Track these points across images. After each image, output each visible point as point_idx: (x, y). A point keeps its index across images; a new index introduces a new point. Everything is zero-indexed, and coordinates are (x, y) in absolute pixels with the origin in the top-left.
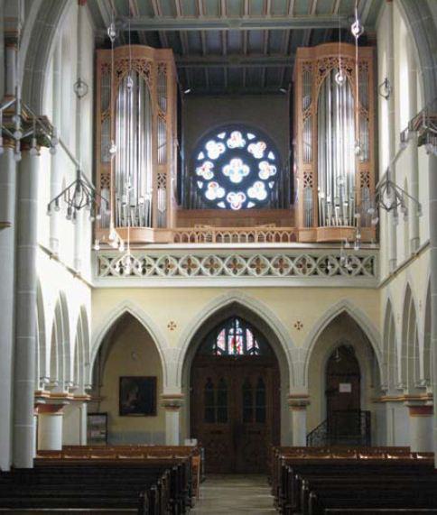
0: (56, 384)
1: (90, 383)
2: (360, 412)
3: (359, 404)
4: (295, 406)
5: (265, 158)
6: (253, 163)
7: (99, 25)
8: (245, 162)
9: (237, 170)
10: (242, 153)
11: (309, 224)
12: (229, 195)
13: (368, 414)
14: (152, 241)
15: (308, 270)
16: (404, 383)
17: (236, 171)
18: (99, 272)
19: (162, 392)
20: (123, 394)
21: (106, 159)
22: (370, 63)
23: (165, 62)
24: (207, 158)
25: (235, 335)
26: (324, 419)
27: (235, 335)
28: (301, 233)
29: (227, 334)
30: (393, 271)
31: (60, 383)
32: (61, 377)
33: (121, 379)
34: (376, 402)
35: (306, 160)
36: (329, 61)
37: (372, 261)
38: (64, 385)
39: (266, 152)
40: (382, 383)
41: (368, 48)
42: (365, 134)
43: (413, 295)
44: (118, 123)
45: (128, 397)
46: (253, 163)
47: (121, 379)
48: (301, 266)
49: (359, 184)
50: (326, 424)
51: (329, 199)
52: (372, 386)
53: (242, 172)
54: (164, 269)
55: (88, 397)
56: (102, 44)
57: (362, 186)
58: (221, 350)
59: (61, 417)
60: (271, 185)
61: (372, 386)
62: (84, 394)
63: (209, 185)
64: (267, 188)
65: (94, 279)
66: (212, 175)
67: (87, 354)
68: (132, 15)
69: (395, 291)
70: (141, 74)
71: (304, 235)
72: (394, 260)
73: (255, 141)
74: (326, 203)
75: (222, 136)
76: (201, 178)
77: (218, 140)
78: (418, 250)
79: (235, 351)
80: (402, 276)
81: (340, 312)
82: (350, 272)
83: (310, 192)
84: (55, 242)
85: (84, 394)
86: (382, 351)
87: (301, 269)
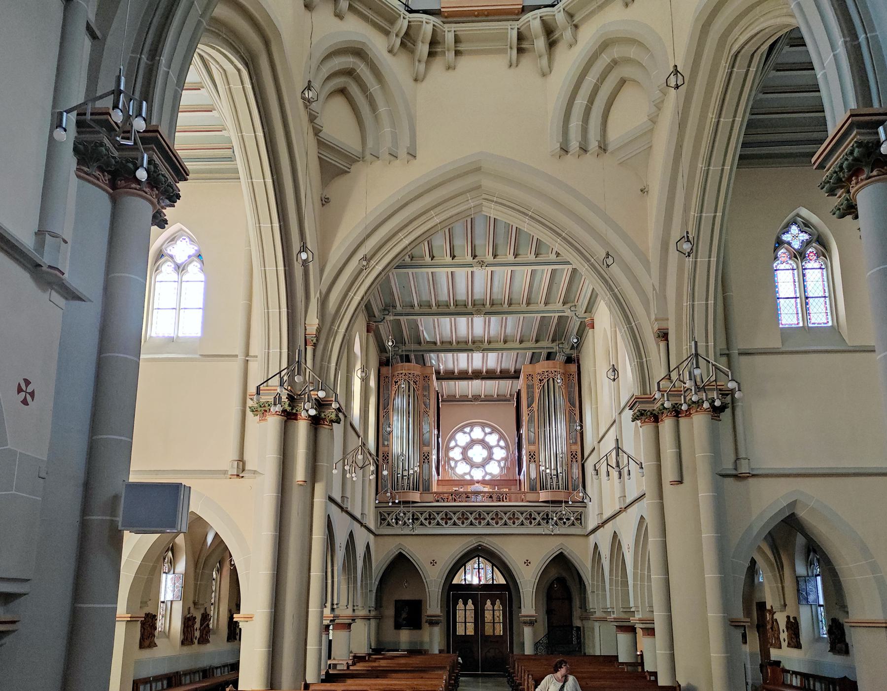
2: (571, 626)
4: (525, 623)
7: (382, 348)
8: (484, 459)
9: (478, 454)
13: (578, 628)
15: (533, 521)
16: (637, 607)
21: (386, 443)
30: (623, 507)
43: (599, 548)
44: (395, 423)
45: (401, 615)
56: (384, 363)
61: (581, 608)
63: (459, 464)
65: (377, 528)
66: (460, 457)
68: (405, 343)
69: (603, 539)
70: (412, 383)
75: (467, 430)
81: (558, 553)
82: (565, 523)
86: (590, 582)
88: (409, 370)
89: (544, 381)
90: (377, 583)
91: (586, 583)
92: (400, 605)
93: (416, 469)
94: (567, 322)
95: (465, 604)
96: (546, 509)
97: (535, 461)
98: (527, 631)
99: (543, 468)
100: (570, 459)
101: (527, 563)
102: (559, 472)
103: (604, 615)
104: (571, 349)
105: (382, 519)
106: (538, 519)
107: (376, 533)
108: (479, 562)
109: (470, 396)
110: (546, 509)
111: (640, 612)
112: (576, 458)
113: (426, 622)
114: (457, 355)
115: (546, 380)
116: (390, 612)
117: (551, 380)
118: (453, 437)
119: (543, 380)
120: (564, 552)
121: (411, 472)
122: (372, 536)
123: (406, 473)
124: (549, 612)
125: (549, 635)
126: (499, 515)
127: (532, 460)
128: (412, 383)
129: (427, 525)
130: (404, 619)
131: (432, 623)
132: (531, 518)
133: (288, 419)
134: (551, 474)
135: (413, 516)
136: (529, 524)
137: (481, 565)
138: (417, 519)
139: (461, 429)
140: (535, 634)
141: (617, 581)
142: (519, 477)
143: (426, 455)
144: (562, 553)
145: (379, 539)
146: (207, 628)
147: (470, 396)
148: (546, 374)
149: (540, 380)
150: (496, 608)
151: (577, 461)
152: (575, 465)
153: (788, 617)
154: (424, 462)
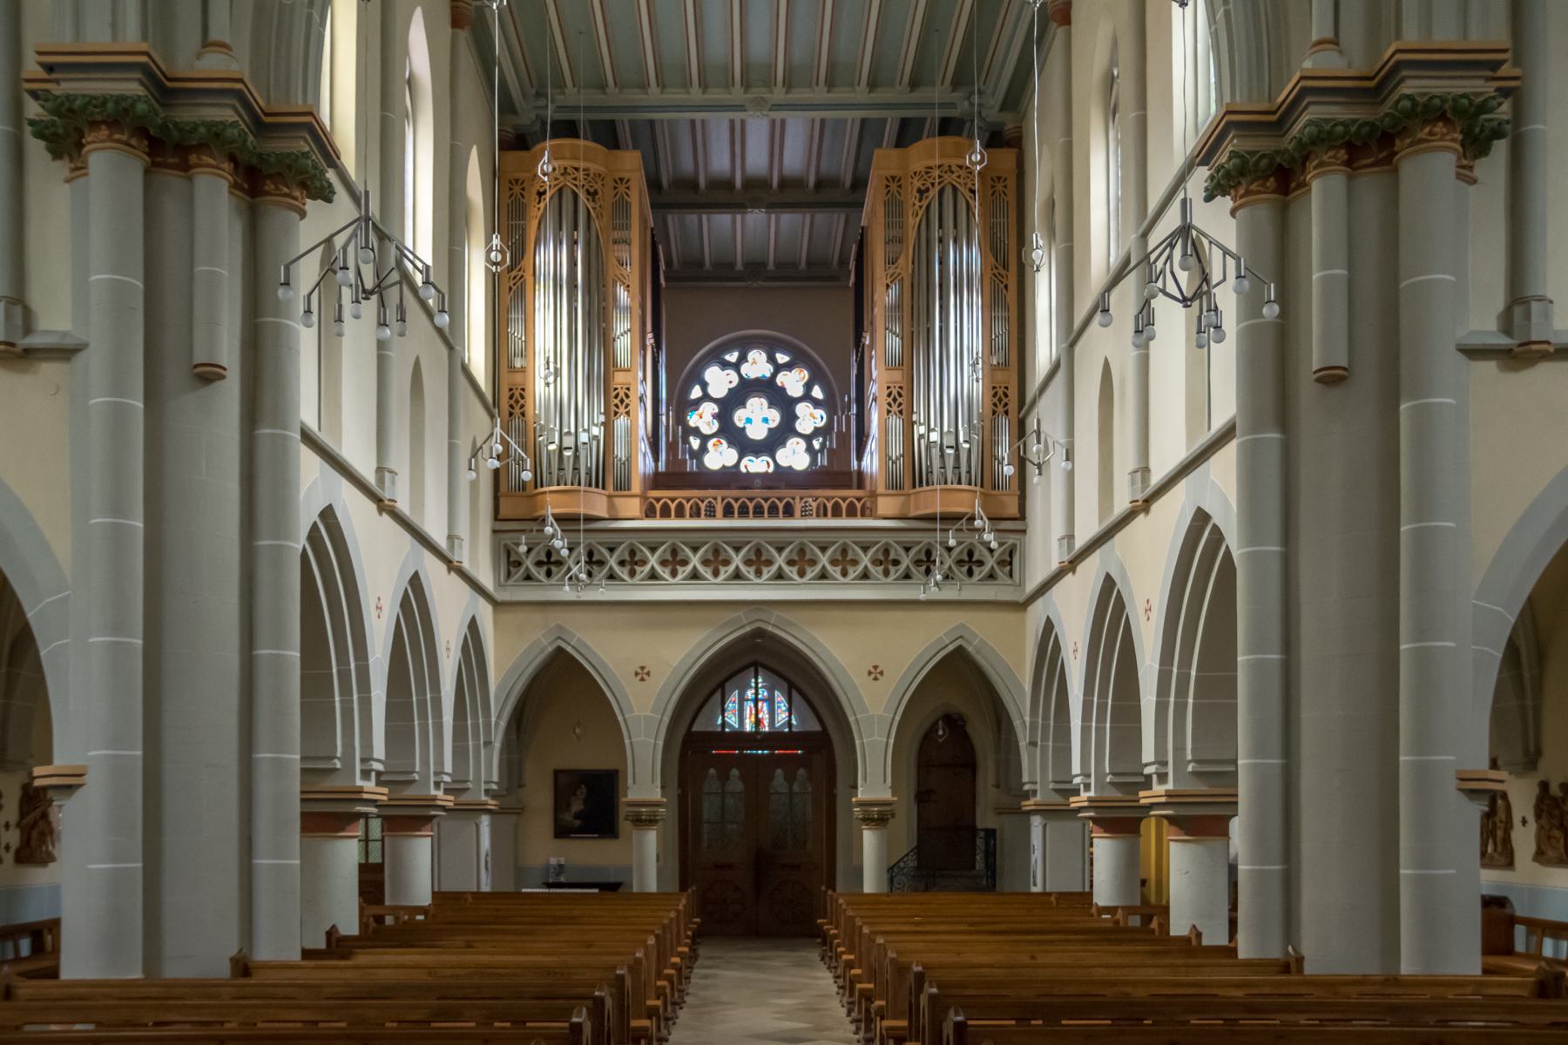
0: (470, 785)
1: (495, 778)
2: (973, 829)
4: (868, 820)
5: (807, 397)
6: (784, 403)
9: (757, 417)
10: (768, 388)
11: (895, 485)
12: (745, 461)
13: (991, 834)
14: (607, 516)
18: (509, 575)
19: (626, 795)
20: (560, 803)
21: (518, 363)
23: (626, 176)
24: (706, 397)
25: (756, 701)
26: (915, 844)
29: (742, 700)
30: (1140, 497)
31: (426, 777)
32: (425, 762)
33: (557, 773)
34: (1000, 814)
37: (1011, 554)
38: (432, 779)
39: (808, 387)
40: (1025, 778)
41: (1010, 150)
42: (999, 329)
44: (540, 302)
45: (569, 805)
46: (784, 403)
47: (557, 773)
48: (881, 563)
50: (916, 851)
51: (934, 437)
52: (997, 786)
55: (492, 804)
57: (994, 412)
58: (731, 726)
60: (816, 444)
61: (997, 786)
64: (809, 449)
66: (715, 426)
67: (487, 725)
70: (582, 196)
71: (886, 505)
73: (789, 366)
74: (929, 445)
75: (732, 357)
76: (696, 432)
78: (1148, 491)
80: (1090, 574)
81: (951, 647)
83: (896, 423)
84: (387, 476)
85: (484, 798)
88: (576, 158)
90: (503, 724)
91: (1017, 723)
92: (566, 783)
93: (595, 431)
94: (994, 25)
95: (724, 777)
96: (925, 538)
97: (901, 412)
99: (922, 430)
100: (989, 407)
102: (961, 439)
103: (1058, 799)
104: (1002, 109)
105: (508, 562)
106: (906, 561)
107: (499, 597)
108: (757, 683)
110: (925, 538)
112: (1006, 405)
114: (708, 219)
115: (937, 188)
116: (540, 797)
117: (949, 191)
118: (697, 377)
119: (927, 190)
120: (965, 644)
121: (584, 437)
123: (569, 441)
124: (923, 797)
125: (920, 850)
126: (808, 551)
127: (895, 408)
128: (582, 196)
129: (626, 577)
131: (641, 822)
132: (886, 560)
133: (154, 164)
134: (942, 444)
135: (590, 554)
138: (601, 563)
139: (716, 357)
140: (886, 847)
141: (1102, 708)
143: (622, 395)
144: (960, 648)
145: (510, 617)
146: (41, 824)
147: (739, 266)
148: (937, 173)
149: (919, 191)
150: (796, 788)
151: (1006, 413)
152: (1004, 423)
153: (1544, 786)
154: (616, 413)
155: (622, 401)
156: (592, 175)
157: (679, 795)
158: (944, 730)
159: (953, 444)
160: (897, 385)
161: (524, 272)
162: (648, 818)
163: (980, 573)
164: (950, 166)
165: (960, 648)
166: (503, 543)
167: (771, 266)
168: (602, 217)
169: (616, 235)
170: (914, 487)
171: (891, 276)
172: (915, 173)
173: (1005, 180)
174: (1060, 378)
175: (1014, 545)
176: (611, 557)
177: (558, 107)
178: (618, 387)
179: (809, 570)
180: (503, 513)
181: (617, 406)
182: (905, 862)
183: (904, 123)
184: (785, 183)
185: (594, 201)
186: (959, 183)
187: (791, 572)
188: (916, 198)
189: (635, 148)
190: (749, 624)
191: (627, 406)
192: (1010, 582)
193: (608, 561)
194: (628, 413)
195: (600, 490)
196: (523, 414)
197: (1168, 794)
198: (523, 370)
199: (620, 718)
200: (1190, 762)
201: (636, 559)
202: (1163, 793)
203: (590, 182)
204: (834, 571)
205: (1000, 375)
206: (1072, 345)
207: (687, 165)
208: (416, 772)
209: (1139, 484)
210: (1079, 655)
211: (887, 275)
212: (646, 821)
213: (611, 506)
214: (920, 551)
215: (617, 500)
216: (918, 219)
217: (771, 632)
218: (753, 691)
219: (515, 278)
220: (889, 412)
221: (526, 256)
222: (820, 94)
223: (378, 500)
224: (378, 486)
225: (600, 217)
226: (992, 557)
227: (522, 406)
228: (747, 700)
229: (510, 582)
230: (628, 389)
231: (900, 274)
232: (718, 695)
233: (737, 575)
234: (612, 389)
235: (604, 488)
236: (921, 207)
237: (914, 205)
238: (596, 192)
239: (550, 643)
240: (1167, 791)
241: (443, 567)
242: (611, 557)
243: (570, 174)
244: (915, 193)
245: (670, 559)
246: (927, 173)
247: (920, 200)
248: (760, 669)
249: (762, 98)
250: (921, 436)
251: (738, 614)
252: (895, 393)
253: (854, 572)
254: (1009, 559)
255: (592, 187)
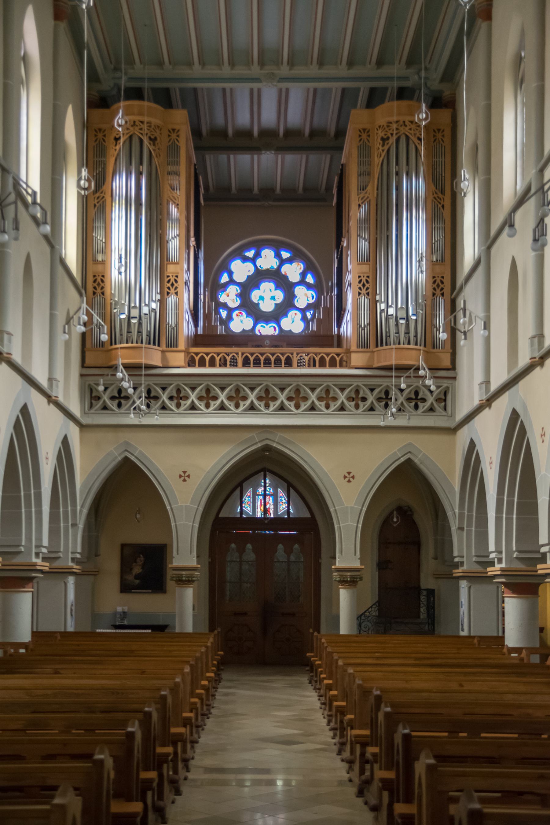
1: (79, 550)
2: (418, 589)
3: (419, 579)
4: (343, 582)
5: (303, 282)
13: (431, 593)
14: (161, 365)
15: (361, 404)
17: (267, 296)
18: (91, 406)
21: (100, 258)
22: (448, 133)
23: (177, 127)
24: (232, 281)
25: (265, 495)
26: (377, 599)
27: (265, 495)
28: (353, 356)
29: (255, 494)
30: (537, 355)
31: (29, 549)
33: (123, 546)
35: (361, 261)
36: (395, 126)
37: (445, 394)
38: (34, 550)
39: (303, 275)
40: (456, 553)
42: (438, 236)
44: (115, 214)
45: (131, 569)
47: (123, 546)
49: (430, 294)
51: (391, 311)
52: (436, 558)
53: (273, 298)
54: (175, 401)
55: (76, 568)
57: (434, 294)
59: (30, 594)
60: (309, 315)
61: (436, 558)
62: (71, 564)
64: (304, 318)
67: (74, 512)
70: (146, 142)
71: (357, 359)
72: (487, 382)
73: (290, 261)
76: (225, 306)
77: (245, 259)
78: (543, 351)
79: (266, 511)
81: (402, 460)
83: (364, 301)
85: (71, 564)
87: (353, 403)
89: (391, 141)
90: (85, 511)
91: (449, 514)
93: (154, 305)
95: (241, 550)
96: (385, 382)
97: (368, 294)
98: (344, 595)
99: (383, 306)
101: (349, 477)
103: (478, 568)
107: (84, 421)
108: (265, 483)
109: (256, 190)
110: (385, 382)
111: (70, 551)
112: (442, 289)
113: (171, 580)
118: (226, 268)
119: (388, 138)
120: (413, 458)
121: (145, 310)
122: (72, 425)
123: (135, 313)
127: (364, 291)
128: (146, 142)
129: (174, 408)
130: (137, 577)
131: (183, 582)
135: (149, 392)
136: (353, 409)
137: (270, 490)
138: (156, 398)
140: (356, 601)
141: (470, 517)
142: (339, 331)
143: (172, 280)
144: (409, 461)
147: (256, 190)
149: (382, 139)
154: (168, 293)
155: (172, 285)
156: (153, 126)
157: (209, 562)
158: (397, 518)
159: (405, 316)
160: (366, 275)
161: (105, 194)
162: (187, 579)
163: (424, 407)
164: (404, 122)
165: (409, 461)
166: (87, 384)
167: (278, 191)
168: (160, 156)
169: (170, 168)
170: (377, 346)
171: (362, 199)
172: (380, 127)
173: (443, 131)
174: (481, 270)
175: (448, 388)
176: (163, 394)
177: (129, 78)
178: (170, 275)
179: (302, 404)
180: (88, 362)
181: (169, 288)
182: (369, 613)
183: (372, 91)
184: (289, 133)
185: (154, 145)
186: (411, 134)
187: (290, 405)
188: (380, 144)
189: (184, 107)
190: (260, 442)
191: (176, 288)
192: (444, 413)
193: (161, 397)
194: (176, 293)
195: (156, 347)
196: (103, 293)
197: (502, 570)
198: (103, 262)
199: (168, 508)
200: (515, 552)
201: (181, 395)
202: (499, 569)
203: (151, 131)
204: (321, 405)
205: (438, 269)
206: (489, 248)
207: (220, 120)
208: (22, 546)
209: (536, 346)
210: (493, 466)
211: (359, 198)
212: (186, 581)
213: (164, 358)
214: (380, 392)
215: (169, 355)
216: (381, 159)
217: (275, 447)
218: (263, 489)
219: (98, 198)
220: (359, 294)
221: (106, 183)
222: (313, 70)
223: (48, 397)
224: (48, 389)
225: (158, 156)
226: (432, 396)
227: (102, 288)
228: (259, 495)
229: (92, 411)
230: (177, 276)
231: (368, 197)
232: (238, 492)
233: (252, 408)
234: (166, 277)
235: (159, 345)
236: (383, 150)
237: (379, 149)
238: (156, 139)
239: (120, 455)
240: (501, 568)
241: (44, 400)
242: (163, 394)
243: (137, 126)
244: (379, 140)
245: (205, 395)
246: (388, 126)
247: (383, 145)
248: (267, 473)
249: (273, 74)
250: (382, 311)
251: (251, 435)
252: (364, 280)
253: (334, 406)
254: (444, 398)
255: (153, 135)
